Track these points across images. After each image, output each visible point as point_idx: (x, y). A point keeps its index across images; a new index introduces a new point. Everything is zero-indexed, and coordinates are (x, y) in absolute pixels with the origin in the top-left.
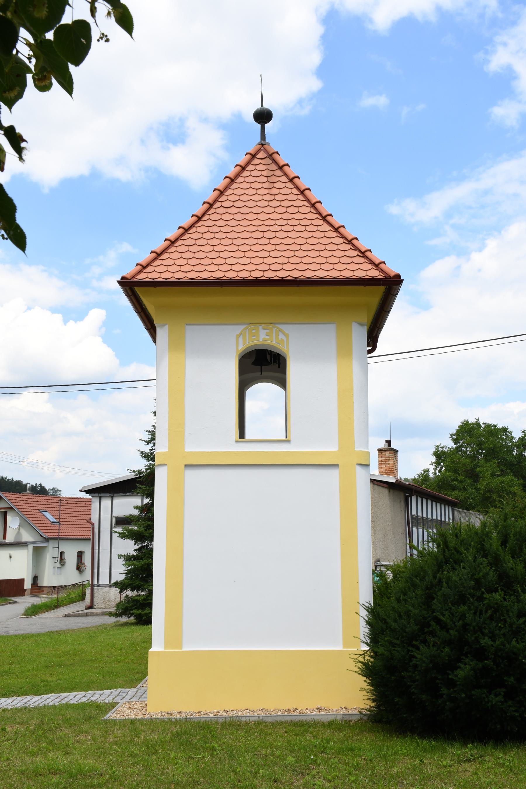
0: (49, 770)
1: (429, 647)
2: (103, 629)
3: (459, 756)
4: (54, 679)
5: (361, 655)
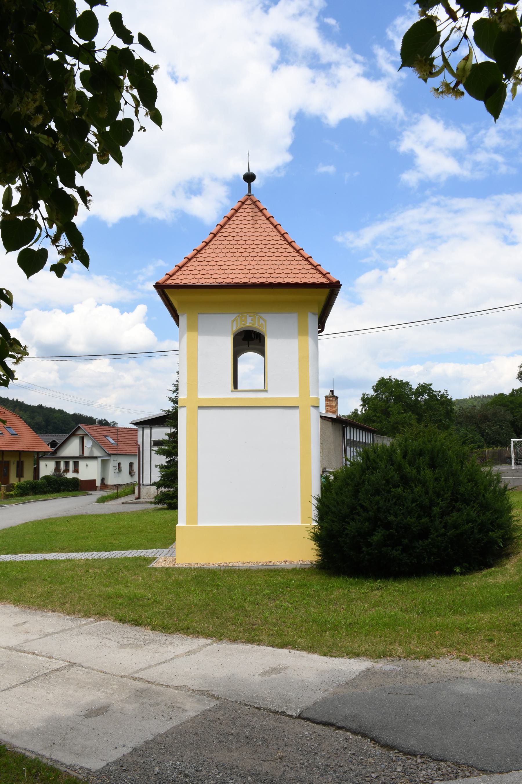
0: (116, 596)
1: (356, 522)
2: (146, 512)
3: (372, 587)
4: (117, 542)
5: (313, 528)
